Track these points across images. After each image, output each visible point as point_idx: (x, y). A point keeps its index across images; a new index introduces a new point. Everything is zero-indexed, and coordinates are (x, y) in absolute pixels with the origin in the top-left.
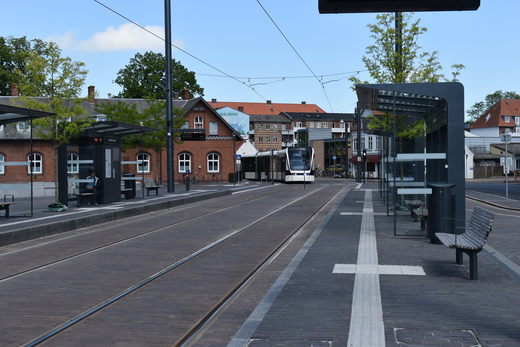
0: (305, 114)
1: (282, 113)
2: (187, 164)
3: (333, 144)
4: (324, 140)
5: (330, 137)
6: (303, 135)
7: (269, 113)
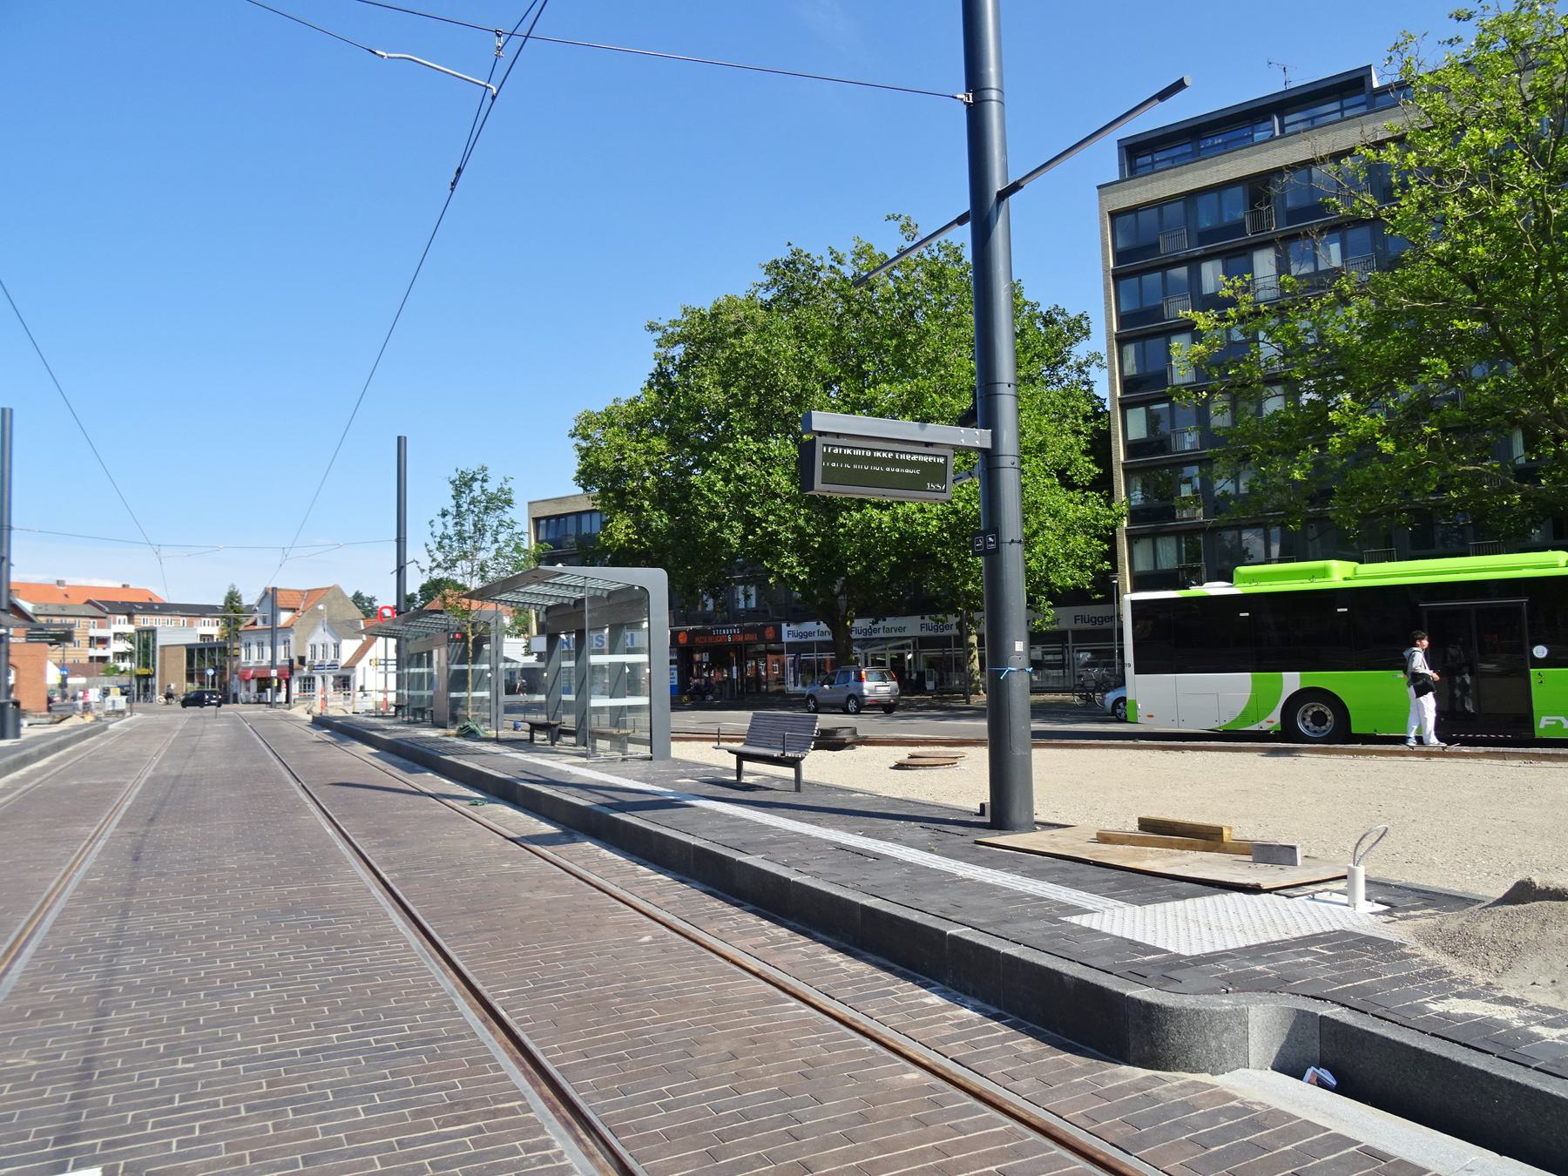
0: (132, 604)
1: (89, 602)
3: (201, 651)
4: (186, 645)
5: (198, 641)
6: (145, 640)
7: (63, 601)
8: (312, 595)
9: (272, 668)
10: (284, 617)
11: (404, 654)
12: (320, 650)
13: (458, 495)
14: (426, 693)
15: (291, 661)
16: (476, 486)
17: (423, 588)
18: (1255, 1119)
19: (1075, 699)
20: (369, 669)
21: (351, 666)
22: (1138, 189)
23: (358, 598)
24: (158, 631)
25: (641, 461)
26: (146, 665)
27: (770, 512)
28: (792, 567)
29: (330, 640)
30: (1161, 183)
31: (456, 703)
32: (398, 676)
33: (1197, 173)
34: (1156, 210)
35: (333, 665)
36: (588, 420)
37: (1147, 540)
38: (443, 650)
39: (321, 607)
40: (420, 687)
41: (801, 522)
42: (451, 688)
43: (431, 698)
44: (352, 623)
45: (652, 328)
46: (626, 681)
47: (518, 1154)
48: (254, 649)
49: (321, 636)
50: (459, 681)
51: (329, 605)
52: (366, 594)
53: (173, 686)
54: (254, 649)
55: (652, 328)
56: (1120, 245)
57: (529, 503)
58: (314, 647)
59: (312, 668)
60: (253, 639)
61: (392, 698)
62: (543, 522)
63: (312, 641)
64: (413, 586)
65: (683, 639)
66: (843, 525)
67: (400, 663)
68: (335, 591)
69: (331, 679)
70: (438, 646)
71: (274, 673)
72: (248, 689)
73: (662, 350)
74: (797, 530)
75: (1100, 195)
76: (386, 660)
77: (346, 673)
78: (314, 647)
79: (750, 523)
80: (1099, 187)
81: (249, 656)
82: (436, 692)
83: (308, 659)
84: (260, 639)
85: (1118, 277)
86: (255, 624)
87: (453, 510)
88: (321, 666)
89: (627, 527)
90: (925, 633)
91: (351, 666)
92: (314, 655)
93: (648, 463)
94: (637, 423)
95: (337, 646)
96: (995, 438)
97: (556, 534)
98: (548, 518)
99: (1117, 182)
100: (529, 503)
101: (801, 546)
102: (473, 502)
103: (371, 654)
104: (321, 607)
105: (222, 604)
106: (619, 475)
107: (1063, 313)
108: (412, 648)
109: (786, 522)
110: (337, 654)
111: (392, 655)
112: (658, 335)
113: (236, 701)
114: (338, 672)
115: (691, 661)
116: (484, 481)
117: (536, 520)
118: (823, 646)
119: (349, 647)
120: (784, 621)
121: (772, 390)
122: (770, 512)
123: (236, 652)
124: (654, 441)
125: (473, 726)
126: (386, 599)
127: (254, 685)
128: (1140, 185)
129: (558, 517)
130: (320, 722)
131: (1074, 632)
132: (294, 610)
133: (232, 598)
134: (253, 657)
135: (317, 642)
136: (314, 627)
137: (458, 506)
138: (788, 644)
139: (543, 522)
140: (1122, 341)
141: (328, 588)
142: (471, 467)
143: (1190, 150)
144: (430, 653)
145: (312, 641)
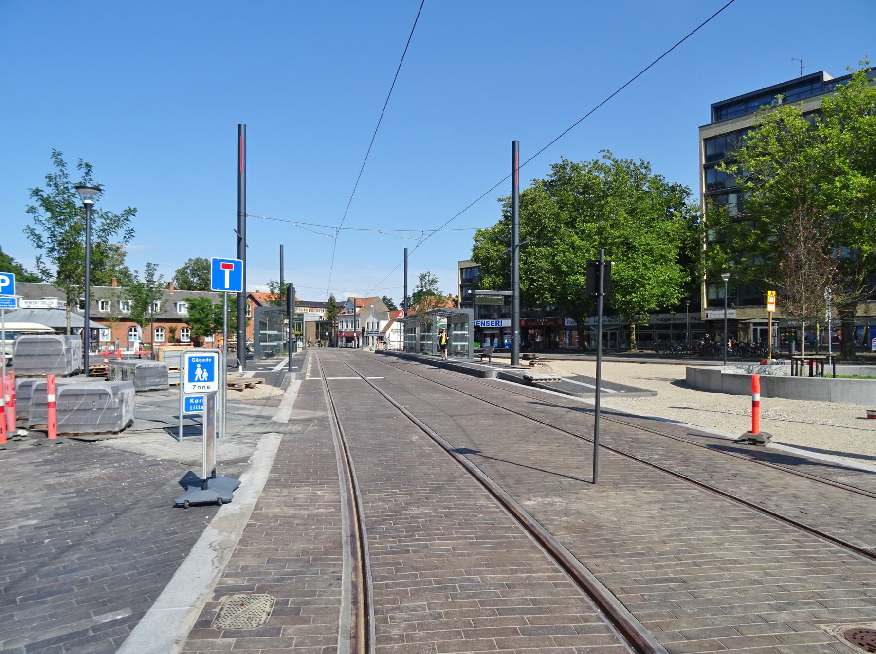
2: (161, 335)
8: (367, 300)
9: (354, 332)
10: (358, 309)
11: (407, 329)
12: (371, 324)
13: (422, 280)
14: (414, 342)
15: (777, 383)
16: (427, 278)
17: (414, 295)
18: (494, 381)
19: (654, 352)
20: (391, 333)
21: (384, 332)
22: (716, 129)
23: (385, 299)
24: (304, 315)
25: (495, 254)
26: (299, 330)
27: (540, 277)
28: (548, 298)
29: (375, 321)
30: (726, 126)
31: (423, 345)
32: (404, 336)
33: (742, 122)
34: (724, 138)
35: (377, 332)
36: (480, 233)
37: (712, 286)
38: (419, 328)
39: (372, 306)
40: (412, 340)
41: (552, 281)
42: (421, 340)
43: (415, 344)
44: (385, 314)
45: (500, 200)
46: (463, 338)
47: (495, 649)
48: (344, 324)
49: (371, 319)
50: (423, 338)
51: (374, 305)
52: (388, 297)
53: (310, 339)
54: (344, 324)
55: (500, 200)
56: (708, 154)
57: (459, 262)
58: (369, 323)
59: (368, 333)
60: (344, 319)
61: (402, 344)
62: (465, 270)
63: (368, 321)
64: (410, 294)
65: (523, 324)
66: (568, 281)
67: (405, 331)
68: (377, 298)
69: (375, 338)
70: (418, 326)
71: (355, 334)
72: (342, 341)
73: (505, 208)
74: (551, 284)
75: (700, 131)
76: (400, 330)
77: (382, 335)
78: (369, 323)
79: (532, 281)
80: (699, 128)
81: (342, 327)
82: (416, 342)
83: (366, 329)
84: (347, 320)
85: (706, 168)
86: (344, 313)
87: (420, 286)
88: (372, 332)
89: (489, 281)
90: (658, 322)
91: (384, 332)
92: (369, 327)
93: (498, 255)
94: (494, 238)
95: (378, 323)
96: (514, 293)
97: (470, 275)
98: (466, 269)
99: (709, 125)
100: (459, 262)
101: (552, 290)
102: (426, 283)
103: (392, 327)
104: (372, 306)
105: (327, 301)
106: (488, 259)
107: (680, 186)
108: (409, 327)
109: (546, 280)
110: (378, 327)
111: (402, 328)
112: (503, 202)
113: (337, 347)
114: (379, 335)
115: (527, 333)
116: (429, 276)
117: (462, 270)
118: (235, 344)
119: (383, 324)
120: (565, 316)
121: (544, 228)
122: (540, 277)
123: (337, 325)
124: (500, 247)
125: (427, 352)
126: (397, 301)
127: (344, 339)
128: (717, 127)
129: (471, 268)
130: (378, 352)
131: (656, 325)
132: (360, 307)
133: (332, 299)
134: (345, 327)
135: (369, 321)
136: (369, 315)
137: (422, 284)
138: (567, 326)
139: (465, 270)
140: (706, 196)
141: (374, 298)
142: (425, 272)
143: (743, 108)
144: (415, 329)
145: (368, 321)
